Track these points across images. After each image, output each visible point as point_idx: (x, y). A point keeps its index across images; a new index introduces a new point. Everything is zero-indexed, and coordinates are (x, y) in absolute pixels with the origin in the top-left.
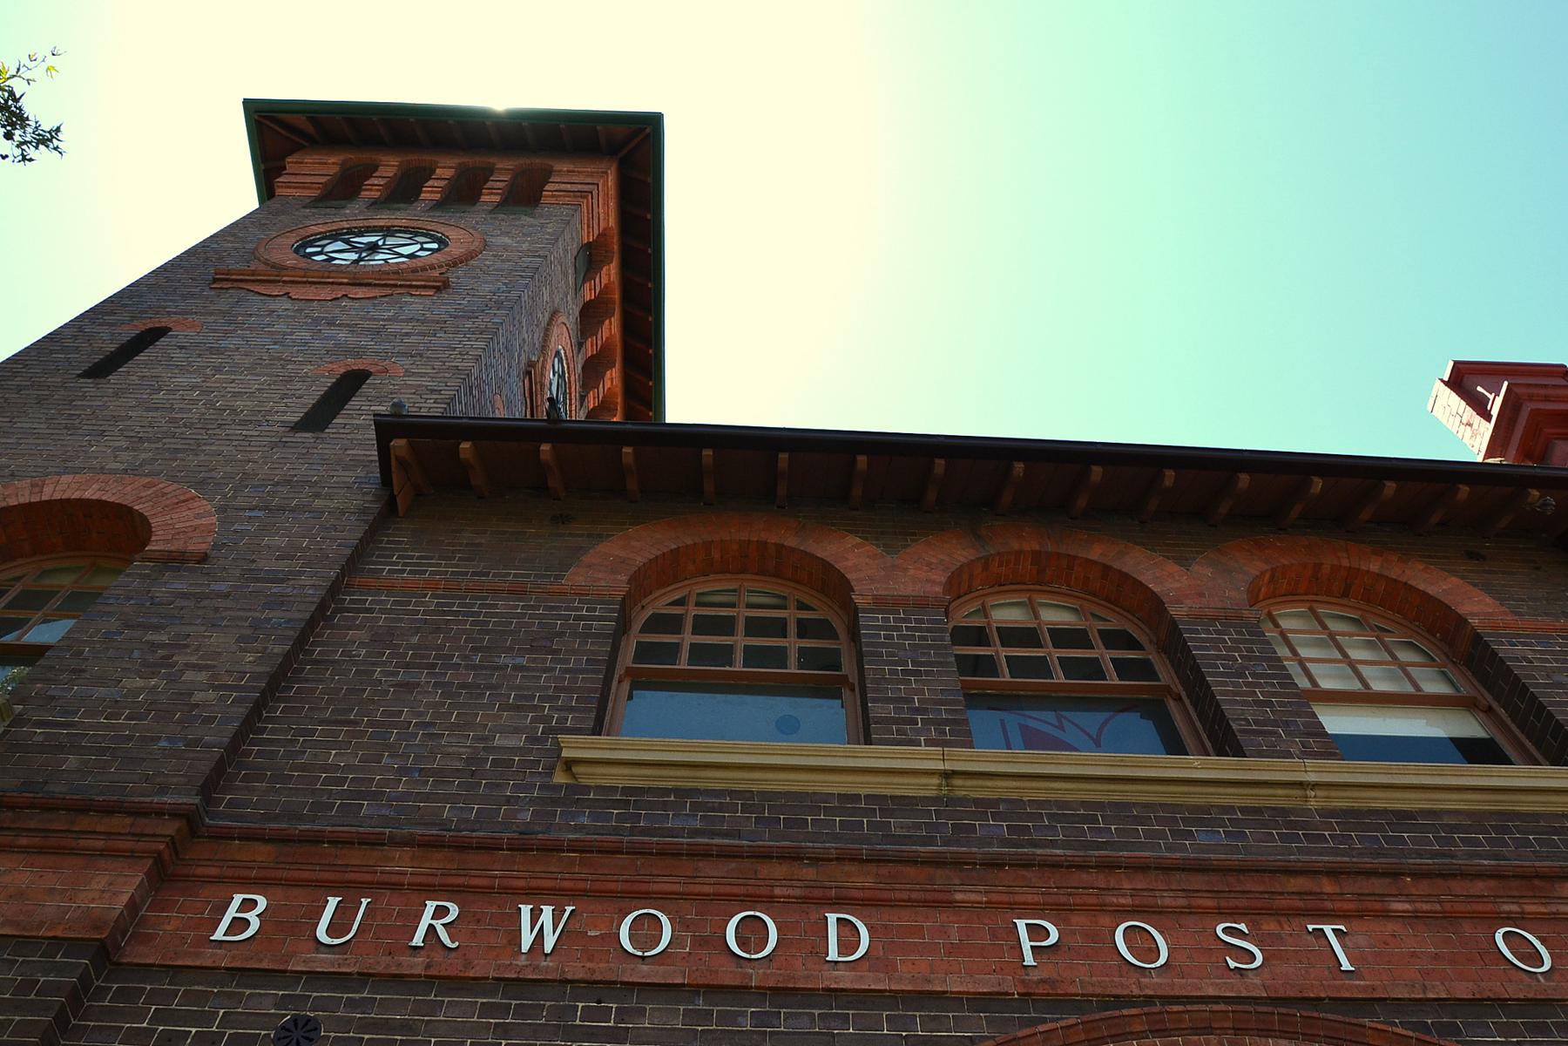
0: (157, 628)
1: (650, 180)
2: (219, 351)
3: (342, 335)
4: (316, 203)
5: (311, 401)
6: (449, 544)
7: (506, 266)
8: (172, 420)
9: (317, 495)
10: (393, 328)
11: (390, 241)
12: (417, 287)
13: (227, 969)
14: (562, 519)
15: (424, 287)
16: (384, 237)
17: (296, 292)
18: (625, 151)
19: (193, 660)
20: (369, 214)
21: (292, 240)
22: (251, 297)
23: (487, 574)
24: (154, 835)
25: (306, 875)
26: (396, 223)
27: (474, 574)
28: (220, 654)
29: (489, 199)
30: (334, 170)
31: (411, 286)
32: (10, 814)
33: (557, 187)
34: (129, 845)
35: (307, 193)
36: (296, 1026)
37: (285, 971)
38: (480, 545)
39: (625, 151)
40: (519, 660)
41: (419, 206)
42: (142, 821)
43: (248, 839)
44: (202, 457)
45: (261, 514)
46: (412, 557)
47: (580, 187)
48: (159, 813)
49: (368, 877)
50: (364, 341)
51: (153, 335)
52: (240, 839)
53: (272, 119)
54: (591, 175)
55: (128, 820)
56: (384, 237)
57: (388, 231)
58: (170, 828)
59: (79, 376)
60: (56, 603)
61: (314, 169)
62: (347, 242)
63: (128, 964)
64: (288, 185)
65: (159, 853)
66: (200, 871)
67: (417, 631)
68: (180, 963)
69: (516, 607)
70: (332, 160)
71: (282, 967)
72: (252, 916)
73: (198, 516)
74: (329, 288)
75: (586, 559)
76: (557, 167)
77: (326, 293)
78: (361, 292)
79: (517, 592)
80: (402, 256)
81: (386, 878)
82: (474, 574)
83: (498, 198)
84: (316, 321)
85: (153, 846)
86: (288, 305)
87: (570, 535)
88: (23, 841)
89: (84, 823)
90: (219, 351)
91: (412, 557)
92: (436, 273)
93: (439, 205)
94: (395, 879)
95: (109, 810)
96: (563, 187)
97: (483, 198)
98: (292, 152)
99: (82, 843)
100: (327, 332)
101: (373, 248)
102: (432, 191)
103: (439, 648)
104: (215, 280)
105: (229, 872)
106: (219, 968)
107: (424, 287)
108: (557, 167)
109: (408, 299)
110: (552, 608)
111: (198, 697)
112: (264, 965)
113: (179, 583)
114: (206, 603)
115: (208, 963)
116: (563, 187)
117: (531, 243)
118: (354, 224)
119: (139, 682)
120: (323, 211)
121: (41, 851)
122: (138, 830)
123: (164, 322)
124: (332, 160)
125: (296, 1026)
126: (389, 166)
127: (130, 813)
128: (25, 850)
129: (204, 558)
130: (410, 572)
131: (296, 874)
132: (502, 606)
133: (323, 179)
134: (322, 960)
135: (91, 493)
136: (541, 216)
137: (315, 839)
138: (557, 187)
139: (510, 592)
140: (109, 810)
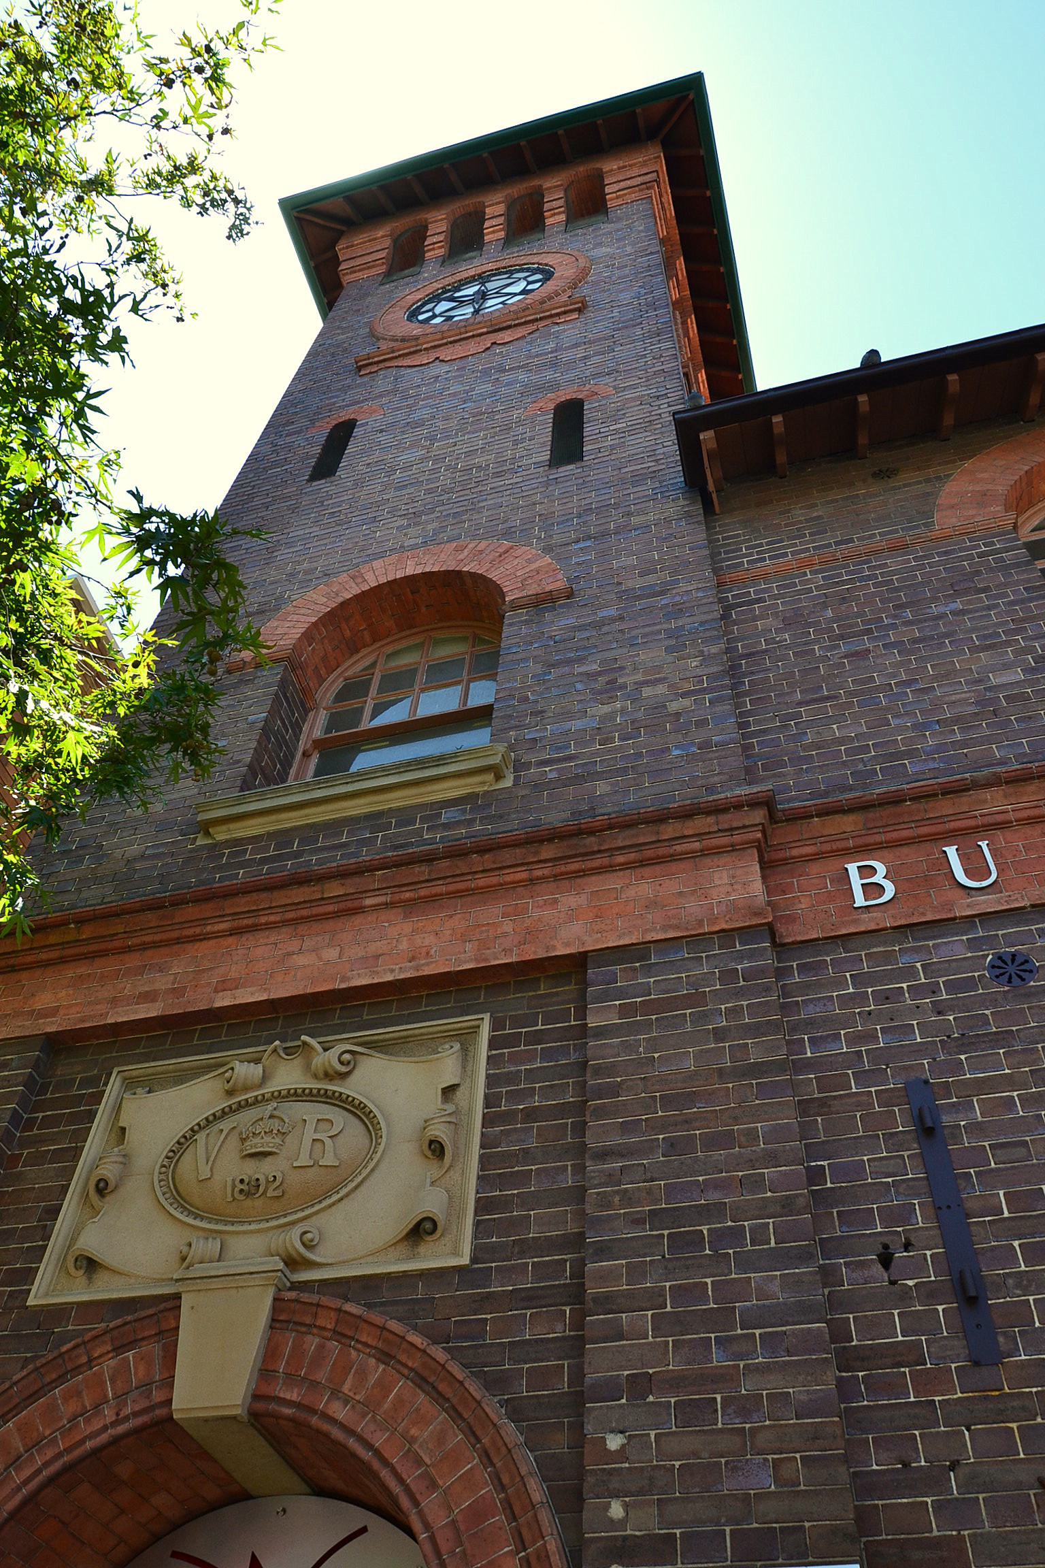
0: (581, 660)
1: (702, 152)
2: (419, 424)
3: (522, 376)
4: (389, 275)
5: (547, 437)
6: (786, 525)
7: (627, 271)
8: (429, 491)
9: (629, 514)
10: (565, 356)
11: (490, 286)
12: (558, 315)
13: (892, 928)
14: (884, 474)
15: (565, 313)
16: (483, 284)
17: (444, 354)
18: (671, 123)
19: (639, 677)
20: (449, 270)
21: (402, 315)
22: (403, 371)
23: (852, 540)
24: (744, 827)
25: (905, 834)
26: (484, 268)
27: (837, 543)
28: (661, 667)
29: (555, 219)
30: (387, 242)
31: (551, 316)
32: (593, 839)
33: (616, 187)
34: (725, 840)
35: (373, 272)
36: (1013, 961)
37: (955, 918)
38: (819, 517)
39: (671, 123)
40: (953, 606)
41: (490, 250)
42: (722, 817)
43: (827, 814)
44: (486, 513)
45: (588, 543)
46: (761, 545)
47: (639, 180)
48: (738, 806)
49: (972, 823)
50: (549, 375)
51: (342, 434)
52: (818, 816)
53: (307, 211)
54: (644, 164)
55: (711, 819)
56: (483, 284)
57: (482, 278)
58: (759, 816)
59: (308, 481)
60: (421, 678)
61: (368, 249)
62: (452, 299)
63: (793, 943)
64: (353, 270)
65: (758, 841)
66: (795, 852)
67: (825, 606)
68: (844, 932)
69: (908, 561)
70: (381, 233)
71: (949, 916)
72: (878, 878)
73: (529, 561)
74: (472, 342)
75: (943, 500)
76: (547, 185)
77: (472, 347)
78: (506, 336)
79: (899, 548)
80: (516, 294)
81: (990, 819)
82: (837, 543)
83: (383, 269)
84: (486, 372)
85: (751, 836)
86: (446, 368)
87: (905, 486)
88: (621, 859)
89: (669, 830)
90: (419, 424)
91: (761, 545)
92: (564, 298)
93: (508, 241)
94: (999, 818)
95: (688, 814)
96: (622, 185)
97: (548, 222)
98: (339, 235)
99: (678, 848)
100: (504, 378)
101: (483, 296)
102: (494, 230)
103: (861, 614)
104: (360, 368)
105: (827, 847)
106: (885, 929)
107: (565, 313)
108: (547, 185)
109: (557, 328)
110: (946, 553)
111: (674, 706)
112: (929, 917)
113: (559, 623)
114: (605, 629)
115: (873, 927)
116: (622, 185)
117: (633, 244)
118: (447, 281)
119: (606, 709)
120: (402, 282)
121: (643, 863)
122: (726, 826)
123: (344, 416)
124: (381, 233)
125: (1013, 961)
126: (439, 225)
127: (708, 813)
128: (625, 866)
129: (570, 594)
130: (771, 558)
131: (895, 835)
132: (893, 563)
133: (383, 254)
134: (985, 902)
135: (411, 569)
136: (619, 219)
137: (895, 800)
138: (616, 187)
139: (891, 549)
140: (688, 814)
